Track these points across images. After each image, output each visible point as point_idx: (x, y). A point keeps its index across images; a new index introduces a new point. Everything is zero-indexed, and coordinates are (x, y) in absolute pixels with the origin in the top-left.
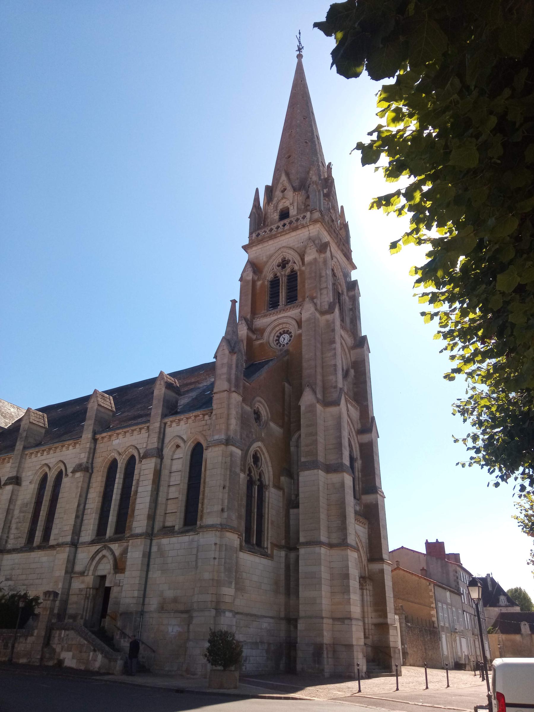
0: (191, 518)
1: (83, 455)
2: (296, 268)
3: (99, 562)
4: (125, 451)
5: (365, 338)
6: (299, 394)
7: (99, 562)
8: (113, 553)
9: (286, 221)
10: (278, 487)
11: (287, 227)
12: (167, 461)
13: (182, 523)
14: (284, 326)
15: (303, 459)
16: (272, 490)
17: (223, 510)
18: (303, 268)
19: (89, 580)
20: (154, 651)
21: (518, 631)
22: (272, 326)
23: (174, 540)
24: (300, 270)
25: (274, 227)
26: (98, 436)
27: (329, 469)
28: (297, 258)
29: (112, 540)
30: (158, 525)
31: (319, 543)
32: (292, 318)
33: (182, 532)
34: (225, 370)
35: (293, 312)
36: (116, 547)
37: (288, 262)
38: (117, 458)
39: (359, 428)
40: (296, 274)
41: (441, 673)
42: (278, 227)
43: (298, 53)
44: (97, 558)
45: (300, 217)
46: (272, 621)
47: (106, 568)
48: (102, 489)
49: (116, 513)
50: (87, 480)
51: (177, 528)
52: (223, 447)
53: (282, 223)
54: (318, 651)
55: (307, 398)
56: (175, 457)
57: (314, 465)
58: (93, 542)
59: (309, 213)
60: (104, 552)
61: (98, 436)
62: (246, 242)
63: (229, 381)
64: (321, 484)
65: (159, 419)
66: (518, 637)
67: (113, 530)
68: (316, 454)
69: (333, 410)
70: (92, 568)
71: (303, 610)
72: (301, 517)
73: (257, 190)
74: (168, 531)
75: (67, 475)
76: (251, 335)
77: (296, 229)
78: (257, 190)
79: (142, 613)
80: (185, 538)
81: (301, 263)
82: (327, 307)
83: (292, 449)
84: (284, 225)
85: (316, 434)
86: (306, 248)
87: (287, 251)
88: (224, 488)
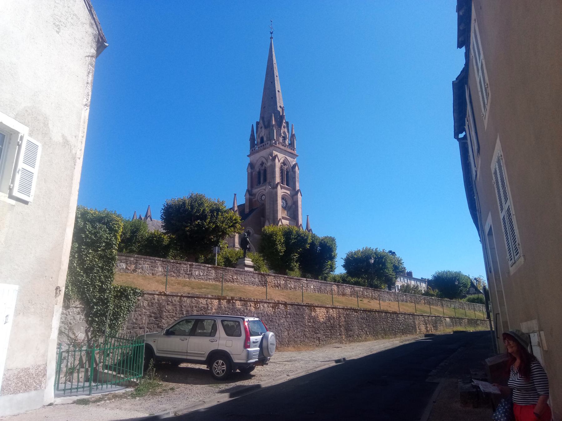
9: (262, 145)
76: (251, 197)
77: (265, 149)
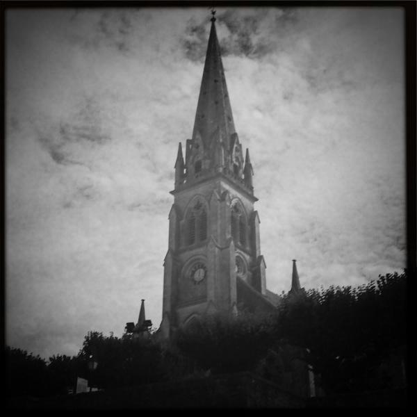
62: (173, 188)
73: (180, 143)
78: (180, 143)
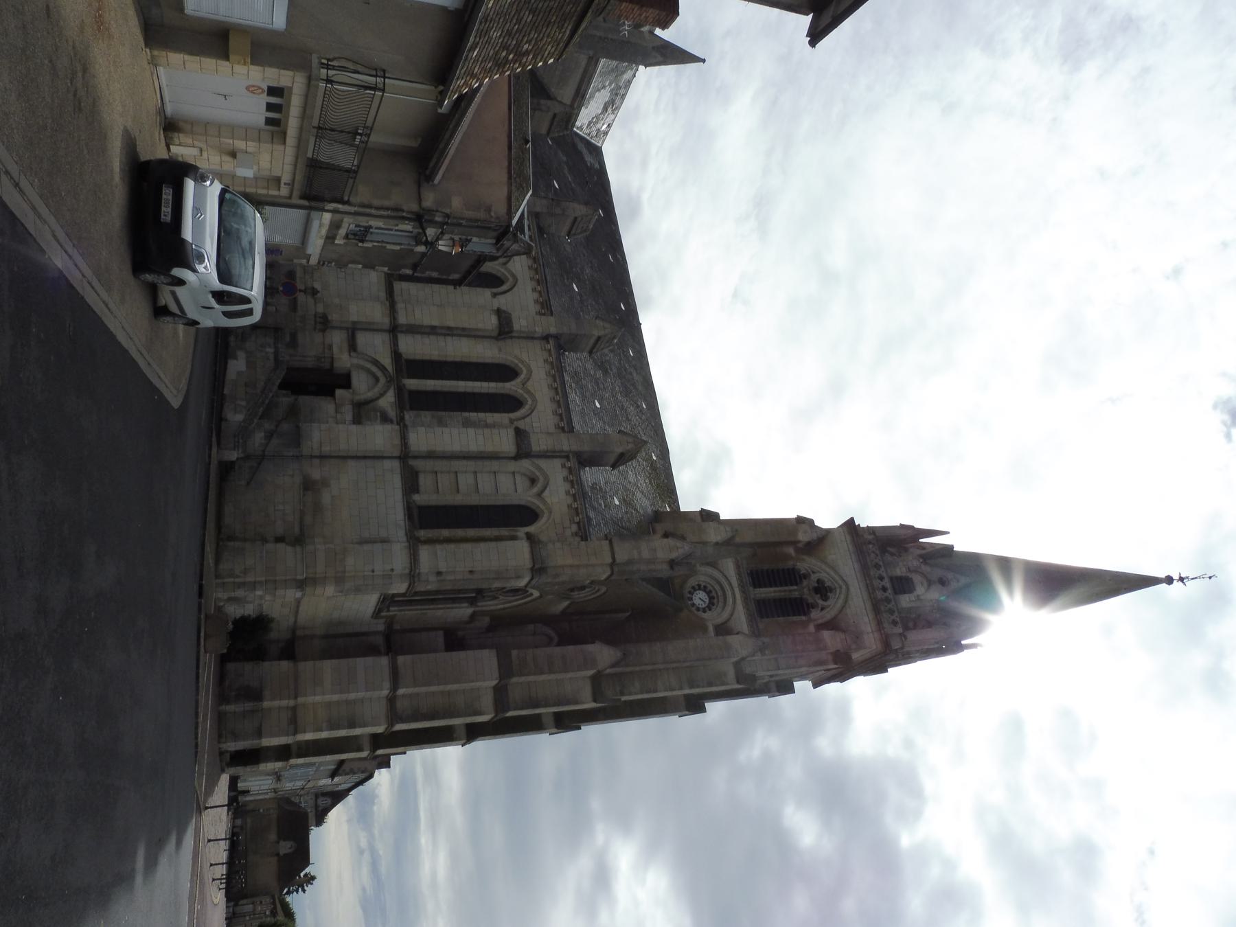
0: (430, 520)
1: (523, 323)
2: (815, 614)
3: (369, 371)
4: (528, 392)
5: (700, 709)
6: (611, 642)
7: (369, 371)
8: (382, 395)
10: (473, 617)
11: (879, 594)
12: (512, 466)
13: (423, 503)
14: (721, 599)
15: (514, 653)
16: (470, 611)
17: (439, 573)
18: (812, 628)
19: (344, 360)
20: (248, 483)
21: (282, 836)
22: (723, 580)
23: (398, 494)
24: (810, 620)
25: (882, 572)
26: (552, 342)
27: (500, 693)
28: (828, 615)
29: (400, 390)
30: (418, 464)
31: (395, 685)
32: (732, 615)
33: (410, 509)
34: (646, 554)
35: (741, 620)
36: (388, 401)
37: (825, 598)
38: (519, 380)
39: (649, 83)
40: (805, 614)
41: (224, 857)
42: (881, 578)
43: (1176, 577)
44: (374, 369)
45: (895, 617)
46: (292, 620)
47: (361, 383)
48: (474, 360)
49: (439, 389)
50: (487, 334)
51: (416, 497)
52: (529, 564)
53: (888, 585)
54: (255, 695)
55: (604, 655)
56: (518, 478)
57: (506, 670)
58: (396, 355)
59: (901, 631)
60: (383, 380)
61: (552, 342)
63: (630, 562)
64: (478, 684)
65: (574, 448)
66: (273, 836)
67: (413, 388)
68: (522, 675)
69: (587, 691)
70: (362, 362)
71: (306, 667)
72: (432, 656)
73: (947, 533)
74: (411, 484)
75: (495, 295)
77: (876, 609)
78: (947, 533)
79: (298, 457)
80: (399, 514)
81: (820, 621)
82: (748, 670)
83: (531, 627)
84: (884, 589)
85: (551, 672)
86: (844, 631)
87: (842, 596)
88: (471, 572)
